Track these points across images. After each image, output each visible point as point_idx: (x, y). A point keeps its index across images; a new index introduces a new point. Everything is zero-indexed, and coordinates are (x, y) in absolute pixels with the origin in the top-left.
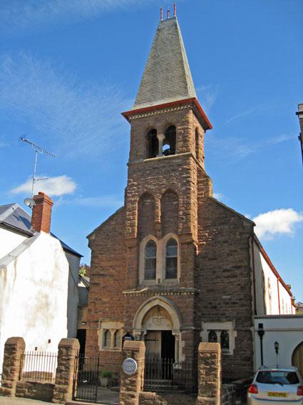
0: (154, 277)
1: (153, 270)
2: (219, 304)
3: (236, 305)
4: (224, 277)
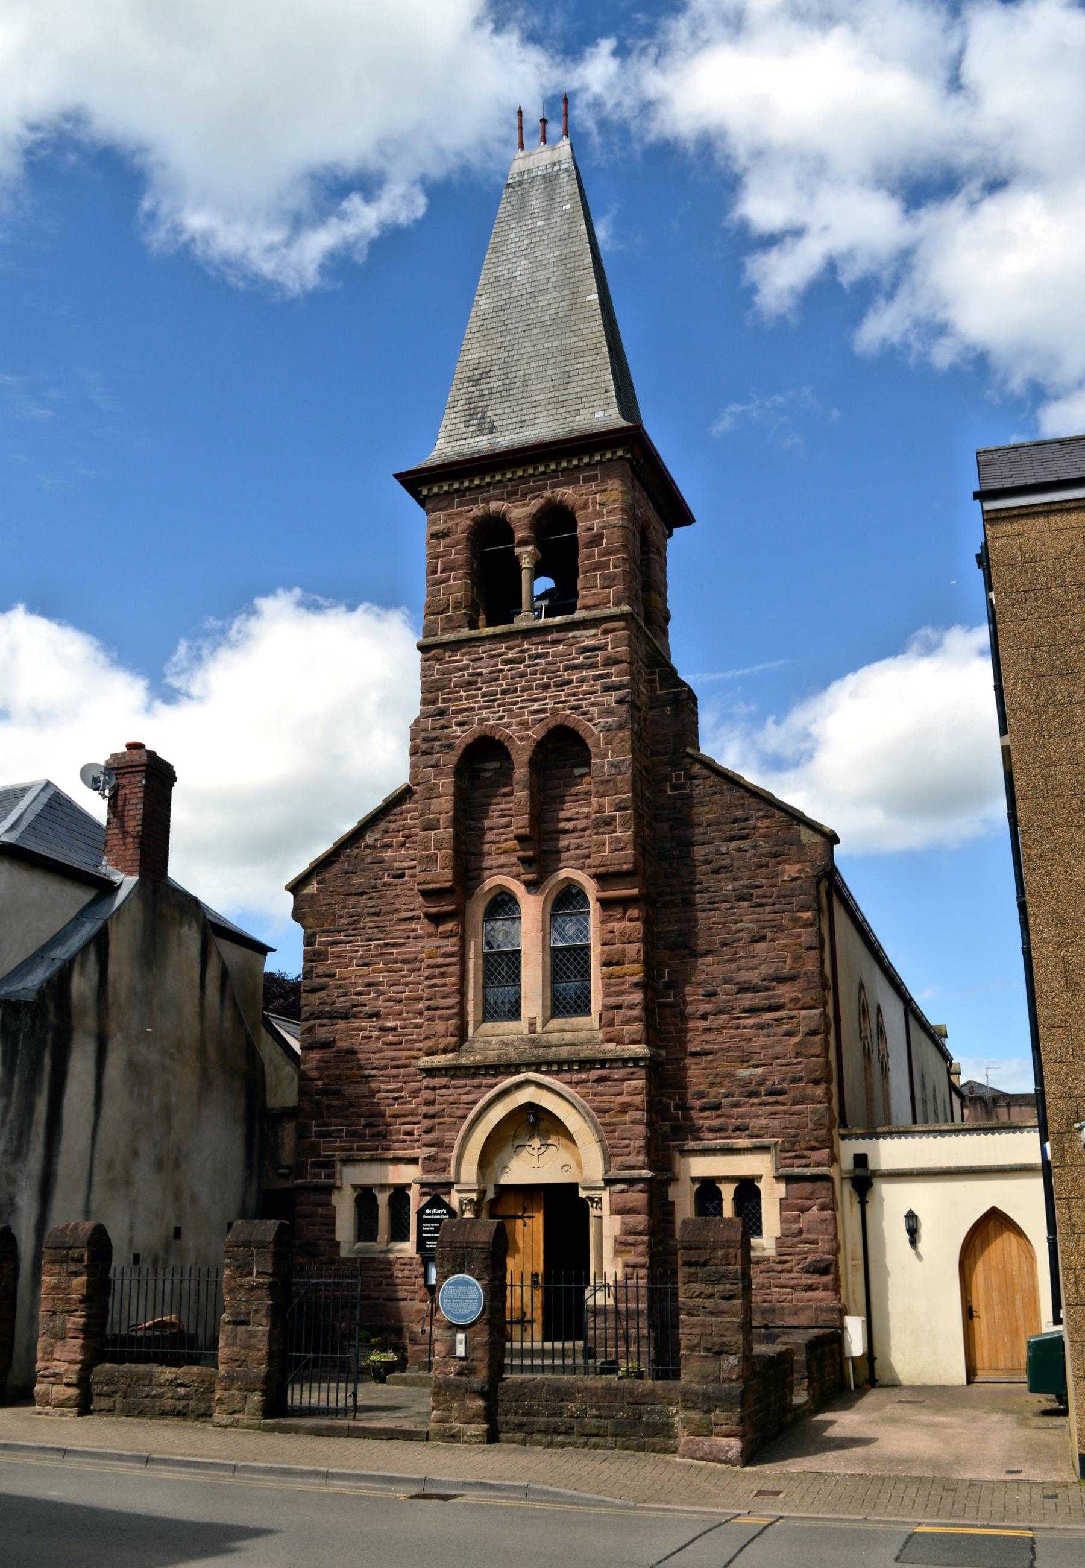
0: (515, 1013)
3: (781, 1098)
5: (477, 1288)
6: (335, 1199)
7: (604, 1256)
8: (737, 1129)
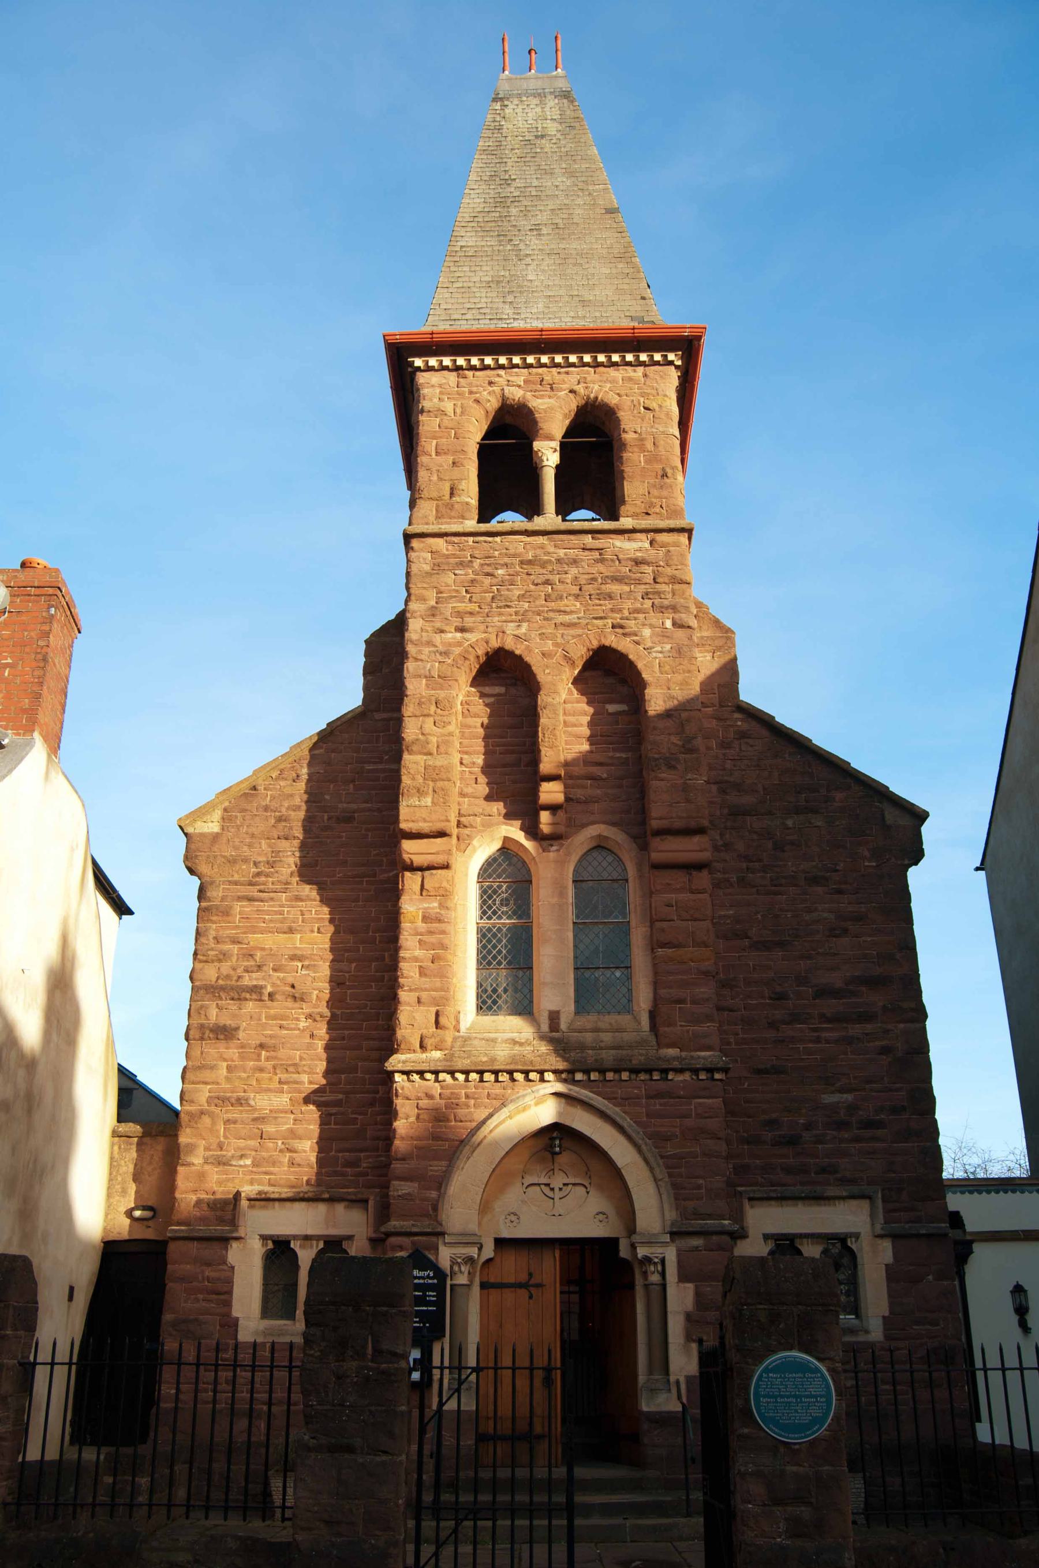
1: (191, 1022)
2: (808, 1127)
3: (880, 1132)
4: (823, 1018)
5: (823, 1376)
6: (234, 1254)
7: (671, 1339)
8: (823, 1170)
